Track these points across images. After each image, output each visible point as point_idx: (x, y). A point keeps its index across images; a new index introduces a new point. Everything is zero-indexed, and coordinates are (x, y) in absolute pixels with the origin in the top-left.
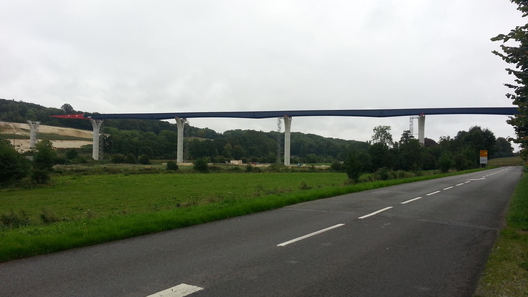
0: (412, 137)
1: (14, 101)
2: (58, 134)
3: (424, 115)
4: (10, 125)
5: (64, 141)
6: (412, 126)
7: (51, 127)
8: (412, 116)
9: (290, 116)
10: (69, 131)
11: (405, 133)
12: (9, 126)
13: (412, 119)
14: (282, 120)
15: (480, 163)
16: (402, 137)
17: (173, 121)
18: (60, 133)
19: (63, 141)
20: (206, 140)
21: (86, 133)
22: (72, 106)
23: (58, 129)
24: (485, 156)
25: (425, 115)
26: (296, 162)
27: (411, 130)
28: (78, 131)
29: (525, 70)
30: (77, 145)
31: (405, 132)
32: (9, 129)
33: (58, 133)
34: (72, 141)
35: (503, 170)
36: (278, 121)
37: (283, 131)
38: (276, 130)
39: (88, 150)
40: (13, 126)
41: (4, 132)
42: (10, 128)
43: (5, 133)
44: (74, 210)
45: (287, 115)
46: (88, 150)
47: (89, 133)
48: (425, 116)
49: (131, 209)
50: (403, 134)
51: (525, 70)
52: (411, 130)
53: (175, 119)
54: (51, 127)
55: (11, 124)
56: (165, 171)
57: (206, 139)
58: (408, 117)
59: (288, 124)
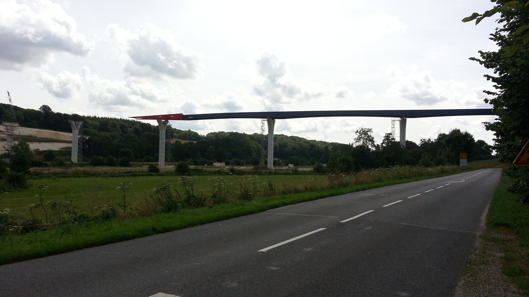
0: (394, 139)
8: (393, 118)
13: (394, 122)
14: (266, 123)
22: (50, 107)
25: (407, 118)
27: (392, 132)
28: (56, 133)
36: (261, 123)
37: (266, 133)
38: (259, 132)
46: (67, 152)
47: (68, 135)
52: (392, 132)
53: (156, 120)
58: (390, 119)
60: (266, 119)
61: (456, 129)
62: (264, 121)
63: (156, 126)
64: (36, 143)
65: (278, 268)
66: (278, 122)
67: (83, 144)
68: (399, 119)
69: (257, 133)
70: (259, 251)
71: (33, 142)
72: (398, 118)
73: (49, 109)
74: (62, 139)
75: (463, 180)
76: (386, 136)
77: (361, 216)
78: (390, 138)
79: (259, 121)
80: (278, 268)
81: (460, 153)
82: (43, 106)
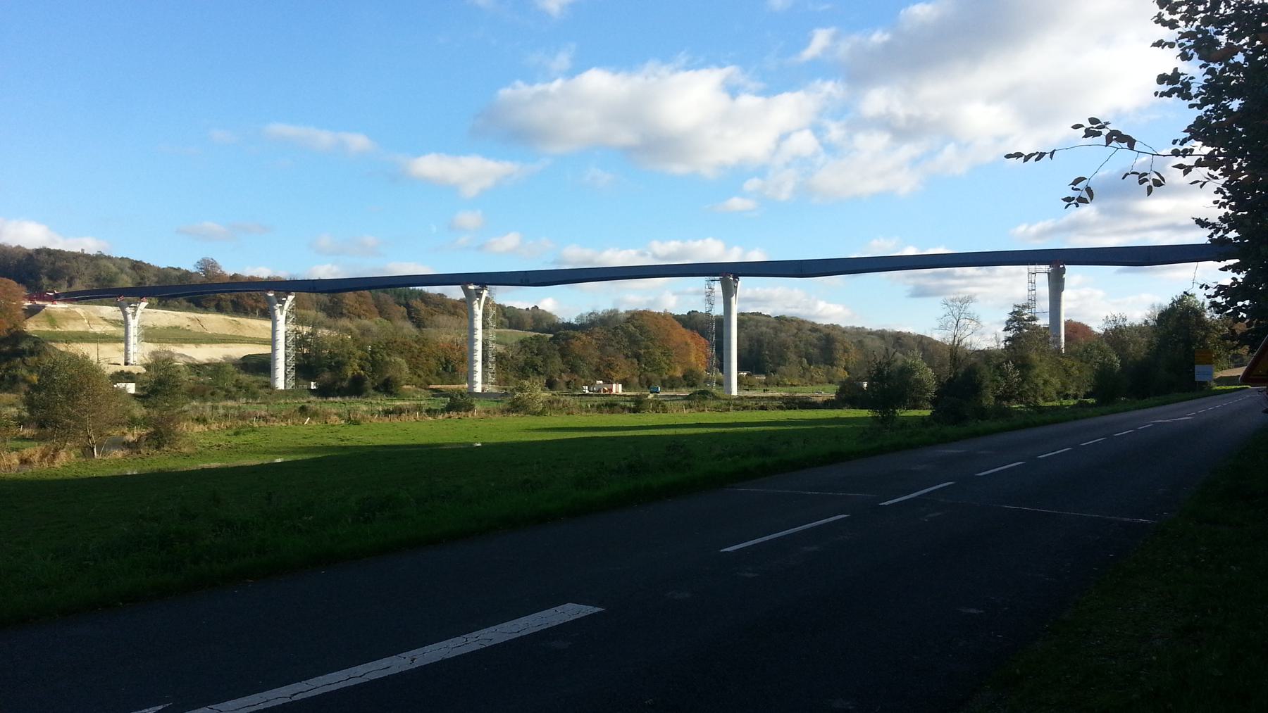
0: (1034, 319)
1: (85, 253)
2: (188, 328)
3: (1061, 266)
4: (77, 311)
5: (202, 345)
6: (1030, 288)
7: (173, 314)
8: (1032, 268)
9: (736, 276)
10: (214, 322)
11: (1017, 310)
12: (76, 312)
13: (1033, 275)
14: (718, 287)
15: (1196, 380)
16: (1010, 320)
17: (455, 293)
18: (195, 328)
19: (201, 347)
20: (535, 336)
21: (258, 326)
22: (217, 261)
23: (189, 318)
24: (1207, 364)
25: (1066, 267)
26: (751, 387)
27: (1030, 302)
28: (234, 322)
29: (1240, 214)
30: (239, 351)
31: (1015, 306)
32: (75, 319)
33: (188, 326)
34: (223, 345)
35: (1248, 396)
36: (707, 287)
37: (718, 310)
38: (702, 309)
39: (262, 366)
40: (84, 313)
41: (63, 327)
42: (78, 318)
43: (66, 330)
44: (704, 297)
45: (728, 273)
46: (262, 366)
47: (261, 325)
48: (1064, 267)
49: (627, 375)
50: (1011, 314)
51: (1240, 214)
52: (1030, 302)
53: (459, 286)
54: (173, 314)
55: (79, 309)
56: (631, 326)
57: (534, 334)
58: (1024, 269)
59: (728, 292)
60: (717, 278)
61: (269, 277)
62: (712, 283)
63: (448, 297)
64: (188, 345)
65: (757, 575)
66: (746, 285)
67: (296, 346)
68: (1045, 268)
69: (696, 311)
70: (1238, 261)
71: (183, 344)
72: (1043, 267)
73: (214, 265)
74: (248, 334)
75: (1188, 416)
76: (1014, 312)
77: (924, 494)
78: (1025, 317)
79: (700, 282)
80: (757, 575)
81: (1196, 380)
82: (204, 260)
